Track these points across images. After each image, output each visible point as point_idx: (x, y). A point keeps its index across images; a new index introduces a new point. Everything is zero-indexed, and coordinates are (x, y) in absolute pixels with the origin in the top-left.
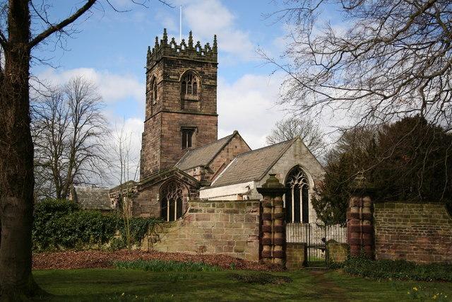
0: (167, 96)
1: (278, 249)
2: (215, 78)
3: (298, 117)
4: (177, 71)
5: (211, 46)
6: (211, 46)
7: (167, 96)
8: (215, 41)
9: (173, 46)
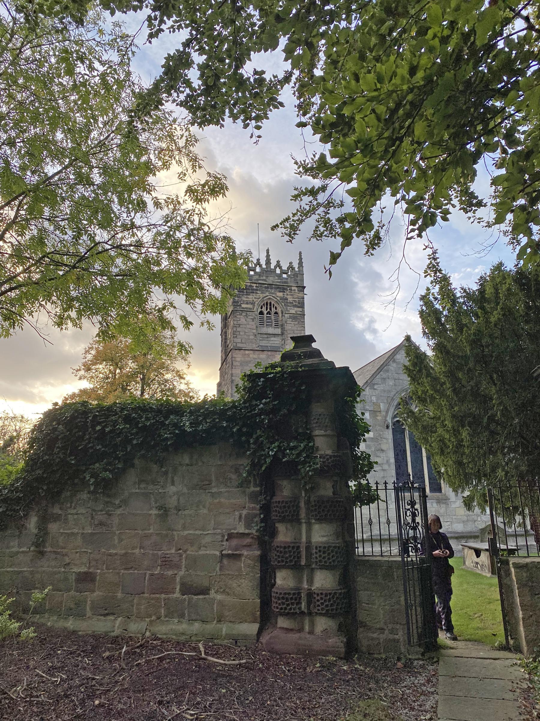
0: (238, 329)
1: (323, 580)
2: (301, 305)
3: (150, 393)
4: (251, 297)
5: (296, 266)
6: (296, 266)
7: (238, 329)
8: (301, 259)
9: (278, 271)
